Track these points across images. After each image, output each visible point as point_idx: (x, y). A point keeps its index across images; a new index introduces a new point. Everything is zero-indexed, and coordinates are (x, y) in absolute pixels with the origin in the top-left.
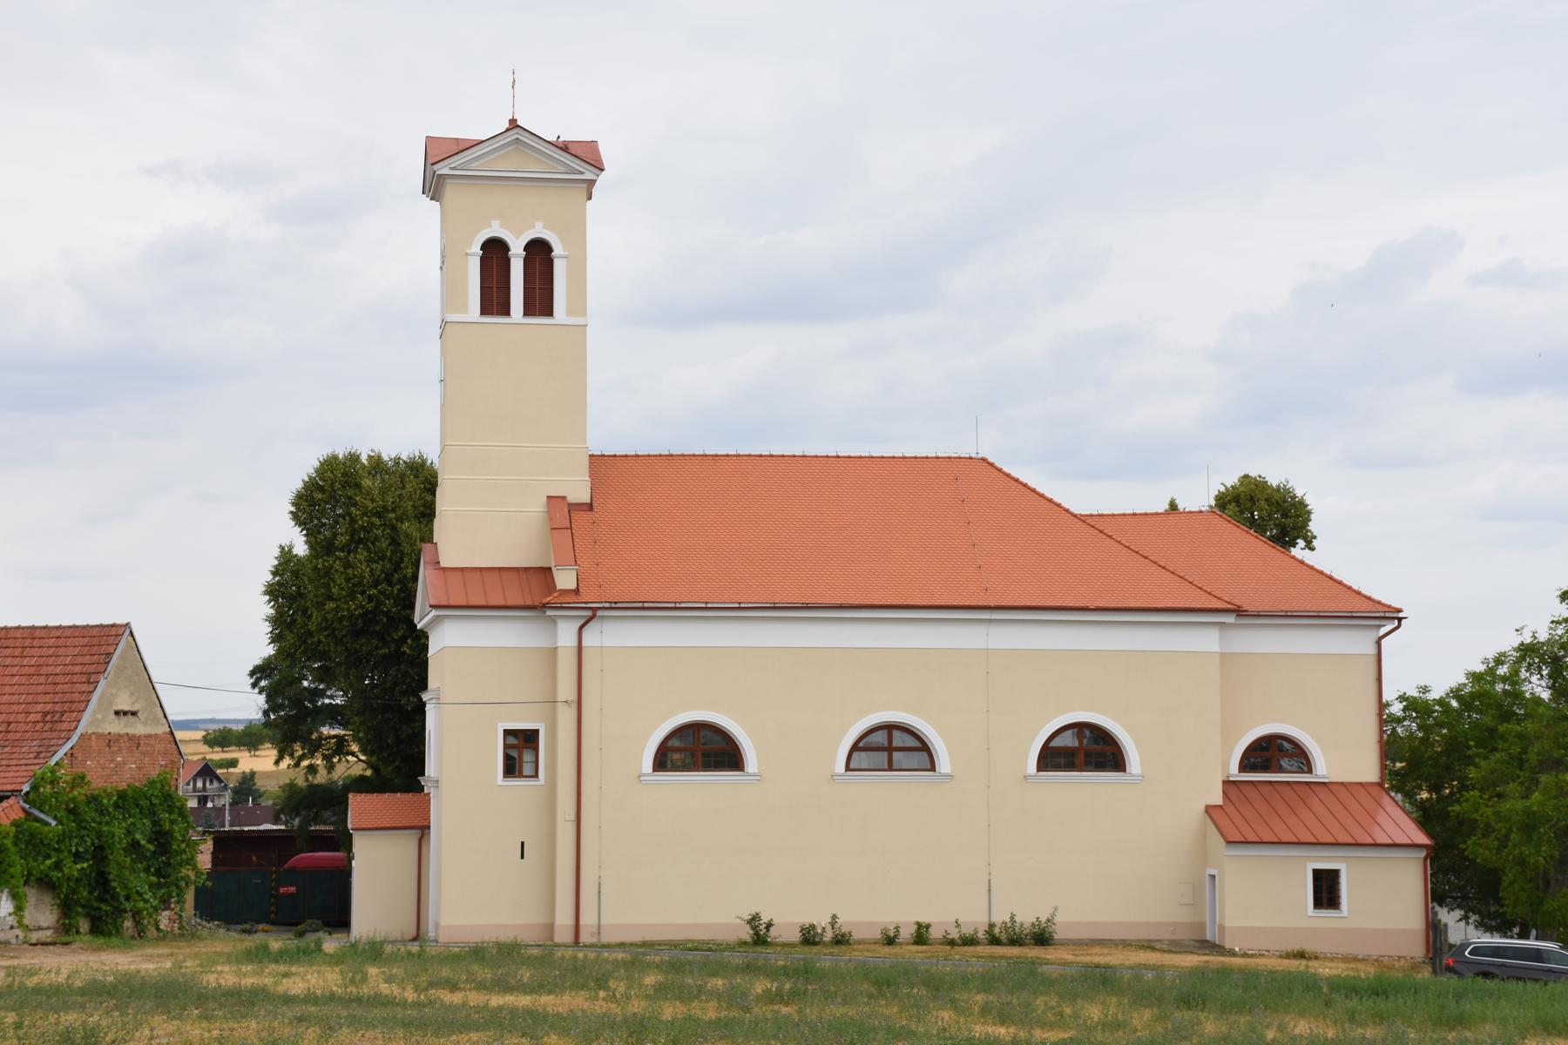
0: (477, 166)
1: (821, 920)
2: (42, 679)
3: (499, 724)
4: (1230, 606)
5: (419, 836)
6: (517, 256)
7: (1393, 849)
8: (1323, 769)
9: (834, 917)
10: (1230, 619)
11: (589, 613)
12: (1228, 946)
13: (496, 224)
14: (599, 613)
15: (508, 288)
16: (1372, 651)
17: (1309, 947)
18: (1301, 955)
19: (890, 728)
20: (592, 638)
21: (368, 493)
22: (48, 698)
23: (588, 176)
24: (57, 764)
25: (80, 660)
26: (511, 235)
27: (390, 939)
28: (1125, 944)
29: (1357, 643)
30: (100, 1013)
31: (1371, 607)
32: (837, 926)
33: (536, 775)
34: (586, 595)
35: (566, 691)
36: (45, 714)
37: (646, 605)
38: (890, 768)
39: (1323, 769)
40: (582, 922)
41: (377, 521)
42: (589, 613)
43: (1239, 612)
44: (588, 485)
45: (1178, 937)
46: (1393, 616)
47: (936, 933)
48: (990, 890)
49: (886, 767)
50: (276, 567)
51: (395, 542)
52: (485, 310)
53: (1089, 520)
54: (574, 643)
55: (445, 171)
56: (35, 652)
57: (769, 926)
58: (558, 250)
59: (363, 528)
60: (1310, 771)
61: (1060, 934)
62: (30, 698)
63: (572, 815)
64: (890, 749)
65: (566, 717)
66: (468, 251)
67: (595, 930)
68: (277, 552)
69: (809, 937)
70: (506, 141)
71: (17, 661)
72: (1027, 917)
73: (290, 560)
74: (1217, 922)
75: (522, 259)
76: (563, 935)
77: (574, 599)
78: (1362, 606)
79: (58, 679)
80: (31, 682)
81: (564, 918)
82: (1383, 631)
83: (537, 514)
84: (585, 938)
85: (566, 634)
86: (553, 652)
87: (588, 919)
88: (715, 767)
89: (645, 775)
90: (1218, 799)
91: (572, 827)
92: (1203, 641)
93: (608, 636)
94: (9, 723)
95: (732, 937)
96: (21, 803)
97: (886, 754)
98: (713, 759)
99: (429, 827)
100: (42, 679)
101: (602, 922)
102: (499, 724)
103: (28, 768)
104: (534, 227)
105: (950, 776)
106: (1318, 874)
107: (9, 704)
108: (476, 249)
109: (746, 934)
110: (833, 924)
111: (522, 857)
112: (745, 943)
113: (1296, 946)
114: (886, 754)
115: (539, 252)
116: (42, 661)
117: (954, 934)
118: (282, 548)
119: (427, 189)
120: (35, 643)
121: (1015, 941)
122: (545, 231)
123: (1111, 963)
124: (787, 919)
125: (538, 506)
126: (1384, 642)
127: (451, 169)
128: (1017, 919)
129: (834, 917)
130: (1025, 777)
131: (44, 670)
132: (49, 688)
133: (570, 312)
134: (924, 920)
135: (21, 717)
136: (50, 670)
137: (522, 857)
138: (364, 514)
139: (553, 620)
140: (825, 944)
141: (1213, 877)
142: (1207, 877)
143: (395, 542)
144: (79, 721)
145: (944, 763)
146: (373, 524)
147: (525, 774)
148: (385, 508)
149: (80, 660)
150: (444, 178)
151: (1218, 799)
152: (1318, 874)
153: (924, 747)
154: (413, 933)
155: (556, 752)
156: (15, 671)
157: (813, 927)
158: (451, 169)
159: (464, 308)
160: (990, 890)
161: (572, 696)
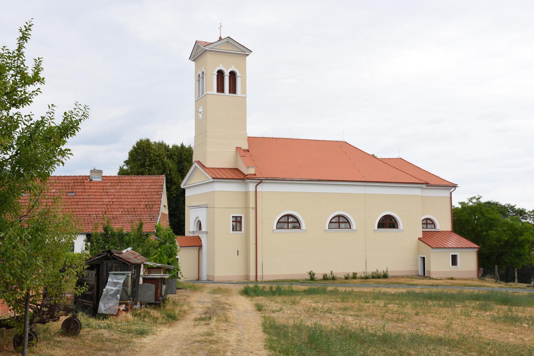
0: (195, 54)
1: (328, 272)
2: (140, 194)
3: (231, 215)
4: (424, 182)
5: (198, 249)
6: (227, 75)
7: (461, 249)
8: (439, 228)
9: (332, 272)
10: (424, 186)
11: (260, 181)
12: (432, 277)
13: (221, 66)
14: (263, 181)
16: (449, 196)
17: (454, 277)
18: (452, 279)
19: (339, 216)
20: (259, 189)
21: (155, 150)
22: (145, 200)
24: (159, 222)
25: (152, 187)
28: (402, 277)
29: (445, 193)
30: (444, 333)
31: (450, 184)
32: (333, 274)
33: (241, 230)
34: (258, 176)
35: (252, 204)
36: (146, 205)
37: (276, 179)
38: (339, 228)
39: (439, 228)
40: (258, 274)
41: (158, 158)
42: (260, 181)
43: (427, 184)
44: (247, 144)
45: (412, 274)
46: (455, 186)
47: (358, 275)
48: (366, 263)
49: (338, 227)
50: (119, 172)
51: (163, 165)
52: (218, 91)
53: (382, 160)
54: (254, 190)
56: (134, 184)
57: (314, 275)
58: (238, 74)
59: (153, 160)
60: (435, 228)
61: (390, 274)
62: (139, 200)
63: (254, 242)
64: (339, 222)
65: (252, 213)
67: (261, 277)
68: (119, 168)
69: (325, 278)
70: (224, 41)
71: (129, 187)
72: (381, 270)
73: (122, 171)
76: (253, 279)
77: (255, 176)
78: (447, 184)
79: (147, 193)
80: (137, 194)
81: (252, 274)
82: (452, 190)
84: (259, 279)
85: (252, 187)
86: (247, 194)
87: (259, 274)
89: (274, 230)
90: (421, 236)
91: (254, 246)
92: (417, 192)
93: (264, 188)
94: (134, 209)
95: (304, 278)
96: (155, 236)
97: (338, 224)
99: (202, 246)
100: (140, 194)
101: (264, 274)
102: (231, 215)
103: (153, 224)
104: (232, 67)
105: (355, 230)
106: (452, 256)
107: (132, 202)
108: (216, 73)
109: (308, 277)
110: (331, 273)
111: (238, 255)
112: (307, 280)
113: (451, 276)
114: (338, 224)
115: (233, 75)
116: (138, 187)
117: (363, 275)
118: (120, 167)
119: (191, 58)
120: (133, 181)
121: (379, 277)
124: (319, 273)
125: (233, 150)
126: (452, 193)
128: (378, 271)
129: (332, 272)
130: (375, 230)
131: (140, 190)
132: (145, 197)
133: (242, 93)
134: (355, 271)
135: (138, 206)
136: (142, 190)
137: (238, 255)
138: (154, 156)
139: (246, 183)
140: (358, 279)
142: (419, 258)
143: (163, 165)
144: (160, 208)
145: (354, 226)
146: (156, 159)
147: (238, 230)
148: (159, 154)
149: (152, 187)
151: (421, 236)
152: (452, 256)
153: (348, 222)
154: (197, 278)
155: (249, 223)
156: (130, 190)
157: (326, 275)
159: (212, 90)
160: (366, 263)
161: (254, 206)
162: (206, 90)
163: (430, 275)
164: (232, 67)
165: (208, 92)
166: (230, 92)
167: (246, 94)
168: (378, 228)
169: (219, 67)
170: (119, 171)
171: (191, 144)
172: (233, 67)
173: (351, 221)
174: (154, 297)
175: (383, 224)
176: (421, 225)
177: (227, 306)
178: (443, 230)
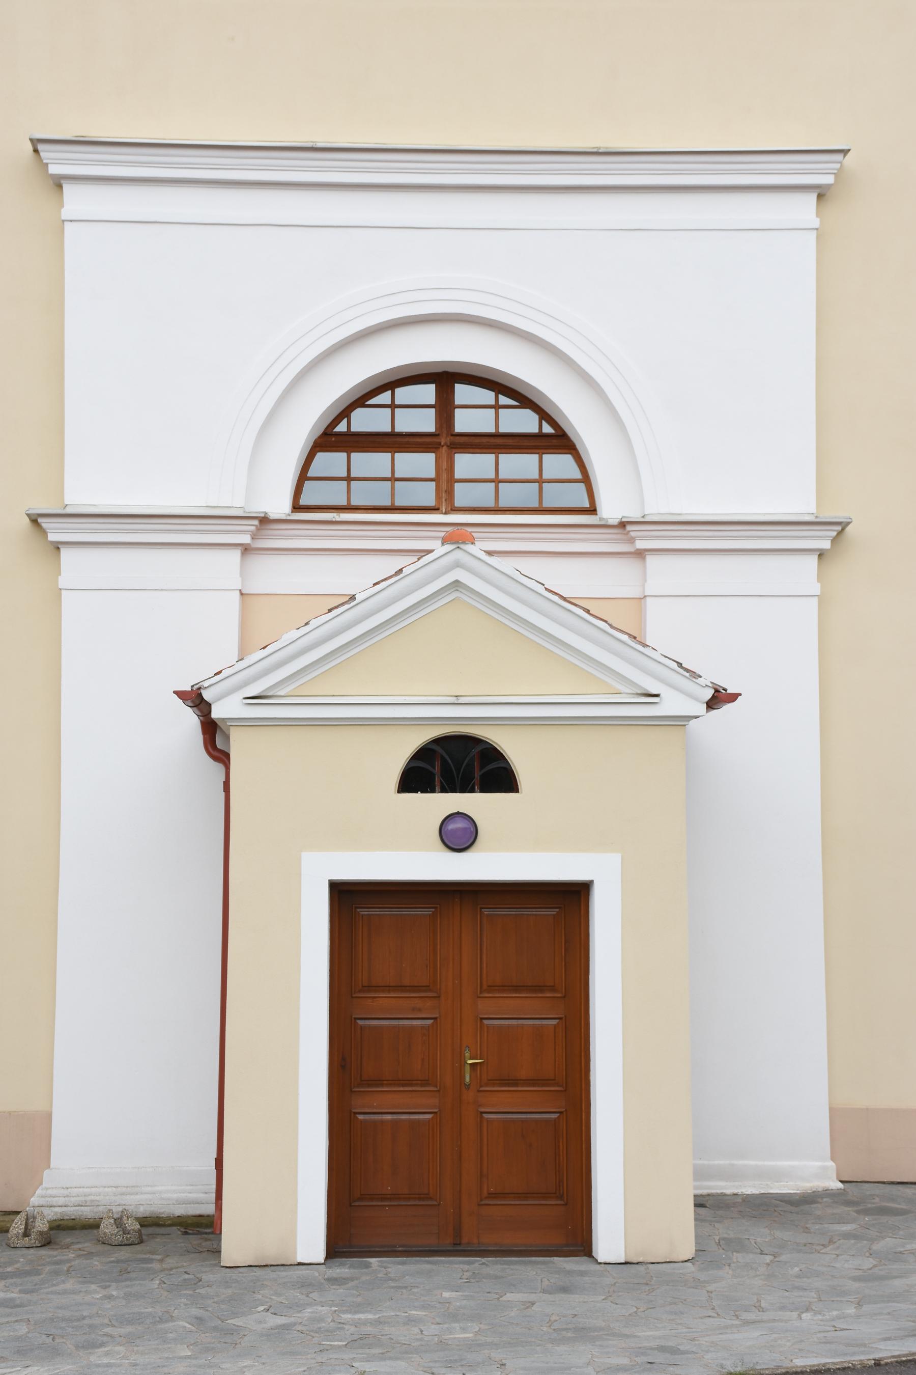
163: (295, 1253)
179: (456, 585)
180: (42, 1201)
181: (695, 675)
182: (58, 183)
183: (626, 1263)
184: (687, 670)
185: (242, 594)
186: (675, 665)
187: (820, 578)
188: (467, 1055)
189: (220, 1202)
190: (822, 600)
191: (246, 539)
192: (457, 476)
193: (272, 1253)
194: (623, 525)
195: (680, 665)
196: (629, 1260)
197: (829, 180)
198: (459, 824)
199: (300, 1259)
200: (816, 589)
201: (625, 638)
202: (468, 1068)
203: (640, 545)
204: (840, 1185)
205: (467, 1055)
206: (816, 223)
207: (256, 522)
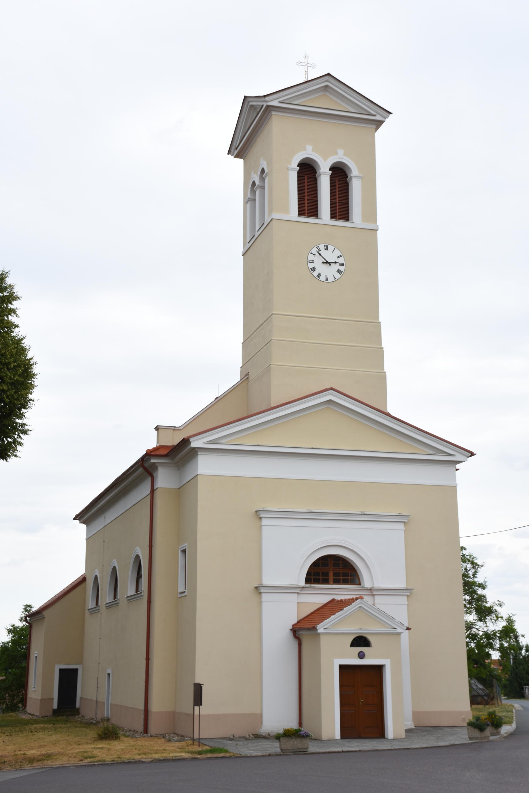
6: (325, 173)
15: (265, 206)
23: (378, 118)
26: (321, 158)
27: (516, 708)
52: (301, 213)
55: (275, 103)
58: (354, 171)
66: (289, 167)
74: (110, 702)
75: (329, 177)
83: (250, 381)
88: (343, 583)
98: (350, 578)
104: (305, 150)
108: (294, 165)
122: (345, 157)
123: (287, 739)
127: (280, 102)
141: (109, 674)
150: (271, 111)
158: (280, 102)
159: (287, 210)
162: (271, 211)
163: (335, 737)
164: (336, 153)
165: (275, 216)
166: (333, 216)
167: (375, 221)
168: (305, 584)
169: (336, 156)
170: (31, 396)
171: (20, 328)
172: (341, 152)
173: (355, 564)
174: (343, 740)
175: (317, 574)
176: (462, 591)
177: (50, 755)
178: (81, 575)
179: (360, 607)
180: (263, 732)
181: (403, 625)
182: (261, 518)
183: (394, 739)
184: (402, 624)
185: (298, 603)
186: (400, 623)
187: (408, 600)
188: (361, 699)
189: (471, 699)
190: (408, 605)
191: (299, 591)
192: (407, 605)
193: (331, 737)
194: (371, 589)
195: (401, 623)
196: (394, 738)
197: (406, 521)
198: (361, 654)
199: (336, 739)
200: (407, 603)
201: (391, 617)
202: (361, 702)
203: (374, 593)
204: (415, 727)
205: (361, 699)
206: (404, 529)
207: (301, 588)
